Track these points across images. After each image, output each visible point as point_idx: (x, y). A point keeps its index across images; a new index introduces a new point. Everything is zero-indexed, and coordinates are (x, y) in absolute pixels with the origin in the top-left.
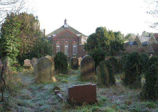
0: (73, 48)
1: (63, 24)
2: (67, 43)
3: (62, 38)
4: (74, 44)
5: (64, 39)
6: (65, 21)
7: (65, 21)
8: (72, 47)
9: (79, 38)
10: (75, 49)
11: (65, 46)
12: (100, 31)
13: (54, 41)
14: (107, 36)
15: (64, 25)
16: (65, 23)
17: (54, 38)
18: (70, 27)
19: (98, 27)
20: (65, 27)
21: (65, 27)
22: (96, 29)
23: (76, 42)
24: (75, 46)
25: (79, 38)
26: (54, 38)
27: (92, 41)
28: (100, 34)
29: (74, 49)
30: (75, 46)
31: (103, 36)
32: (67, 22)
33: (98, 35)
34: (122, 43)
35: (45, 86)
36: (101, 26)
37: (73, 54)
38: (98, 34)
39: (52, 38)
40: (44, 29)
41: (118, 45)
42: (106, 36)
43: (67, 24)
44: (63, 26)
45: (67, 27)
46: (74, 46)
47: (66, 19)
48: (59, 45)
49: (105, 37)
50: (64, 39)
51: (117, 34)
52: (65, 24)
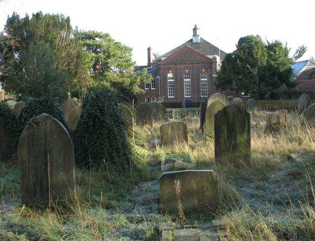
0: (200, 83)
1: (189, 36)
2: (204, 73)
3: (178, 64)
4: (202, 75)
5: (183, 66)
6: (195, 30)
7: (195, 30)
8: (199, 82)
9: (212, 63)
10: (204, 86)
11: (185, 80)
12: (247, 45)
13: (162, 71)
14: (259, 54)
15: (191, 37)
16: (195, 35)
17: (161, 65)
18: (204, 40)
19: (243, 37)
20: (194, 41)
21: (194, 41)
22: (239, 41)
23: (206, 70)
24: (205, 79)
25: (212, 63)
26: (161, 65)
27: (228, 67)
28: (244, 52)
29: (169, 87)
30: (205, 79)
31: (252, 56)
32: (198, 32)
33: (242, 55)
34: (282, 70)
35: (192, 159)
36: (249, 35)
37: (169, 97)
38: (241, 53)
39: (160, 65)
40: (148, 47)
41: (274, 74)
42: (257, 55)
43: (198, 35)
44: (191, 40)
45: (199, 41)
46: (203, 79)
47: (197, 25)
48: (189, 77)
49: (255, 56)
50: (182, 65)
51: (273, 48)
52: (193, 36)
